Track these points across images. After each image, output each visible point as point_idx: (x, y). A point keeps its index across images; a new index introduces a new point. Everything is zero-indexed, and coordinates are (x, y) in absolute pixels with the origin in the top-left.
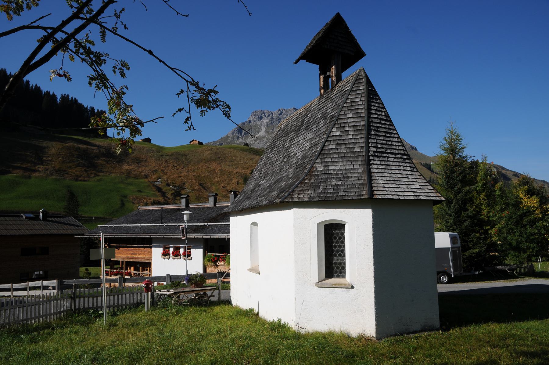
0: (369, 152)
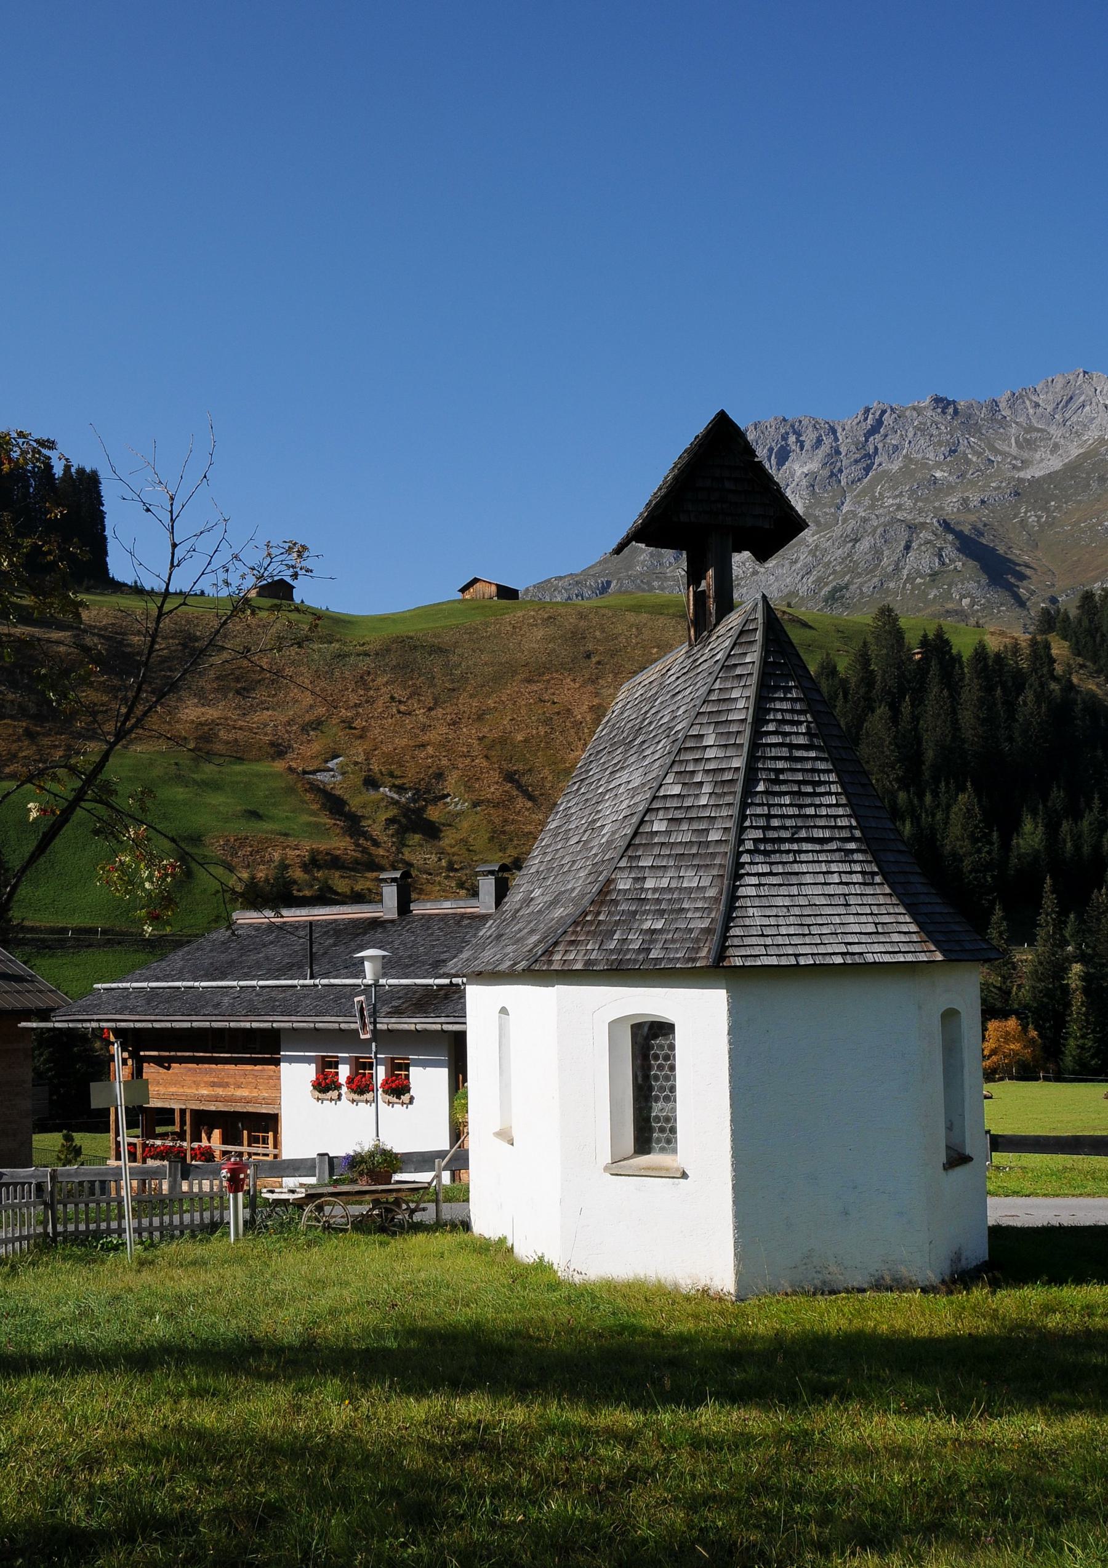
0: (741, 842)
